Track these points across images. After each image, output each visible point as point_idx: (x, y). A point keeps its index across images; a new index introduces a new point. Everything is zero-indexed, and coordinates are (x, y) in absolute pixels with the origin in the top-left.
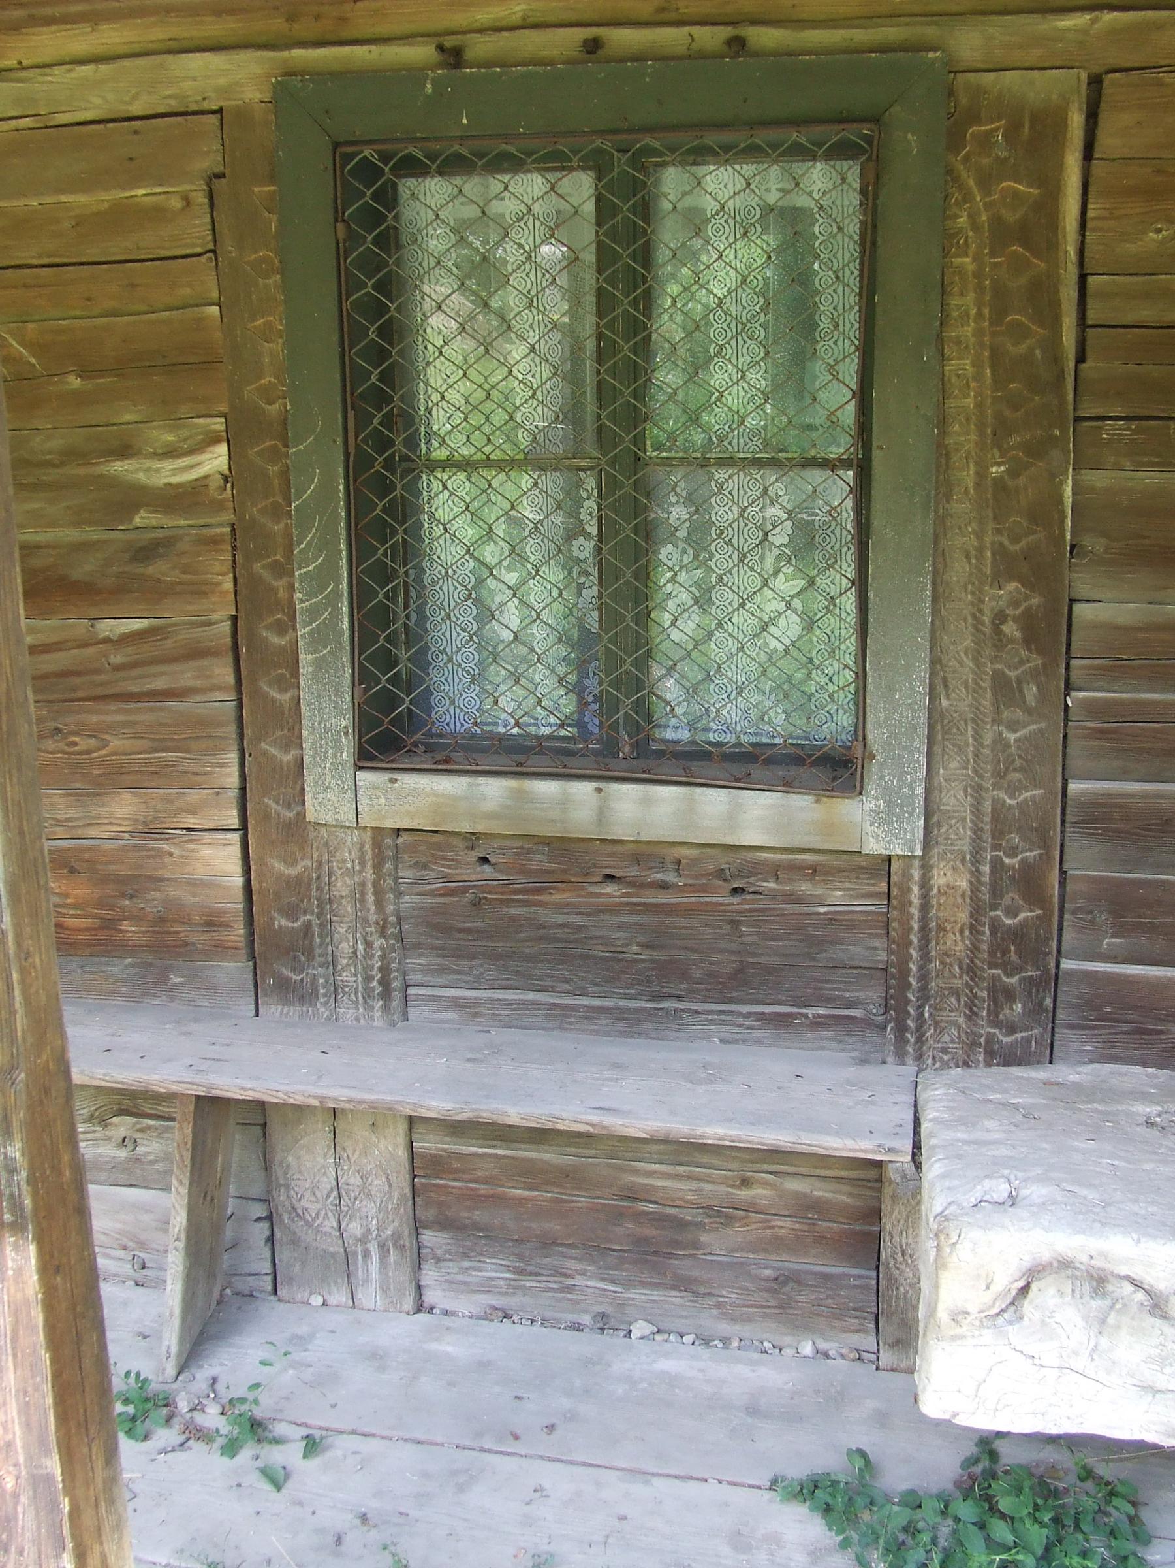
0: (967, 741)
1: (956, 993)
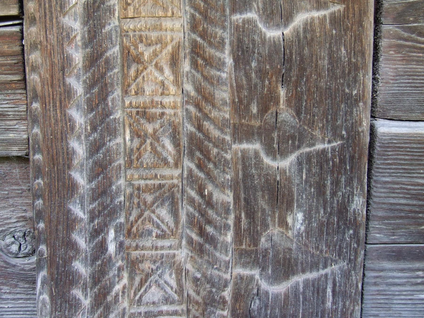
1: (169, 197)
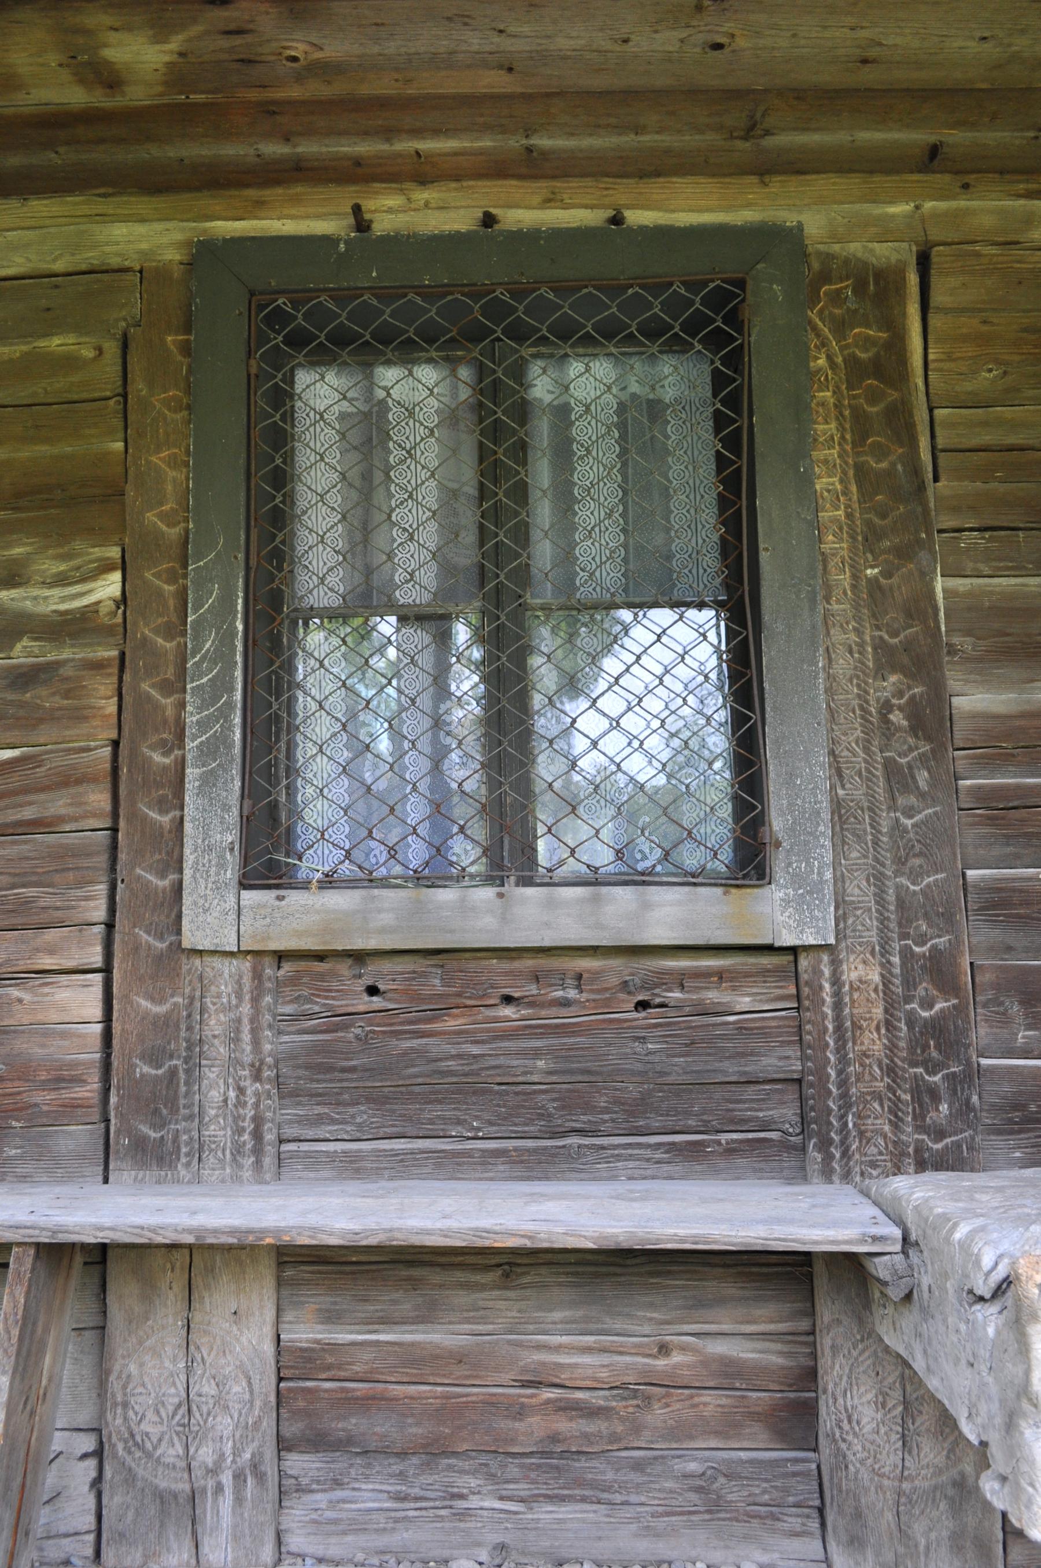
0: (865, 831)
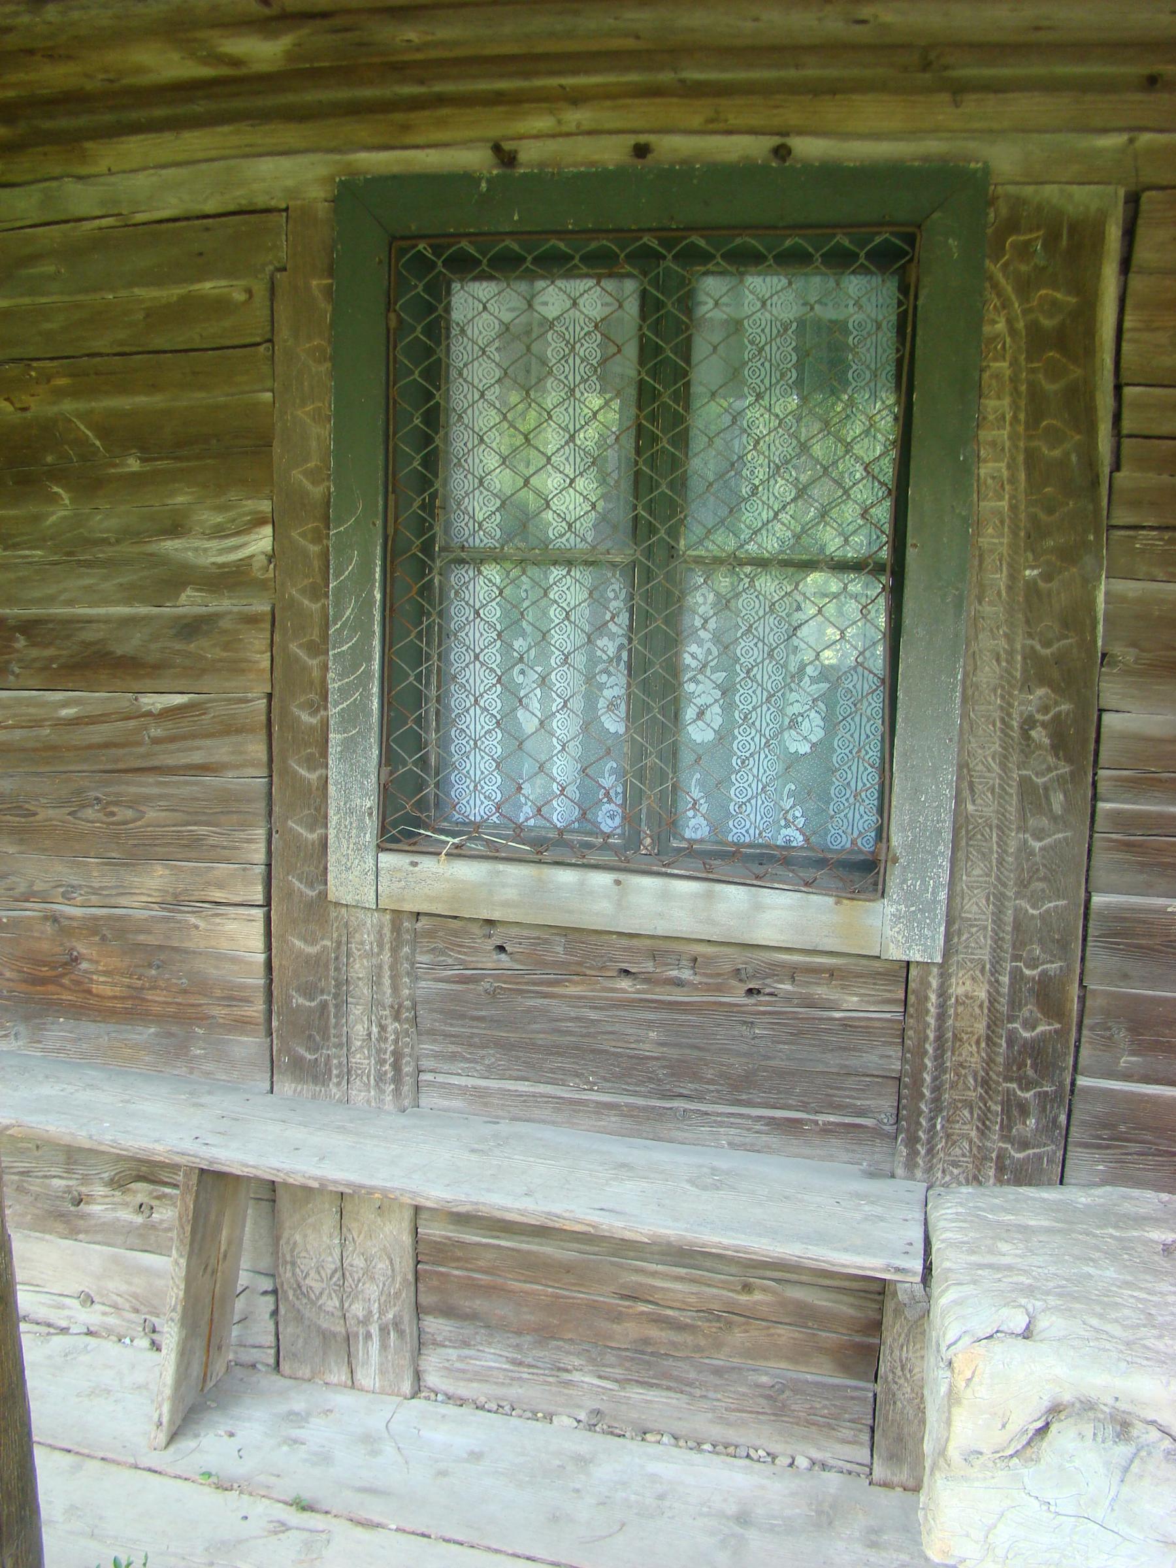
0: (991, 850)
